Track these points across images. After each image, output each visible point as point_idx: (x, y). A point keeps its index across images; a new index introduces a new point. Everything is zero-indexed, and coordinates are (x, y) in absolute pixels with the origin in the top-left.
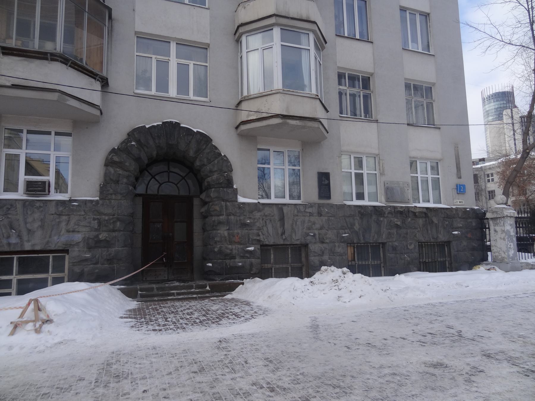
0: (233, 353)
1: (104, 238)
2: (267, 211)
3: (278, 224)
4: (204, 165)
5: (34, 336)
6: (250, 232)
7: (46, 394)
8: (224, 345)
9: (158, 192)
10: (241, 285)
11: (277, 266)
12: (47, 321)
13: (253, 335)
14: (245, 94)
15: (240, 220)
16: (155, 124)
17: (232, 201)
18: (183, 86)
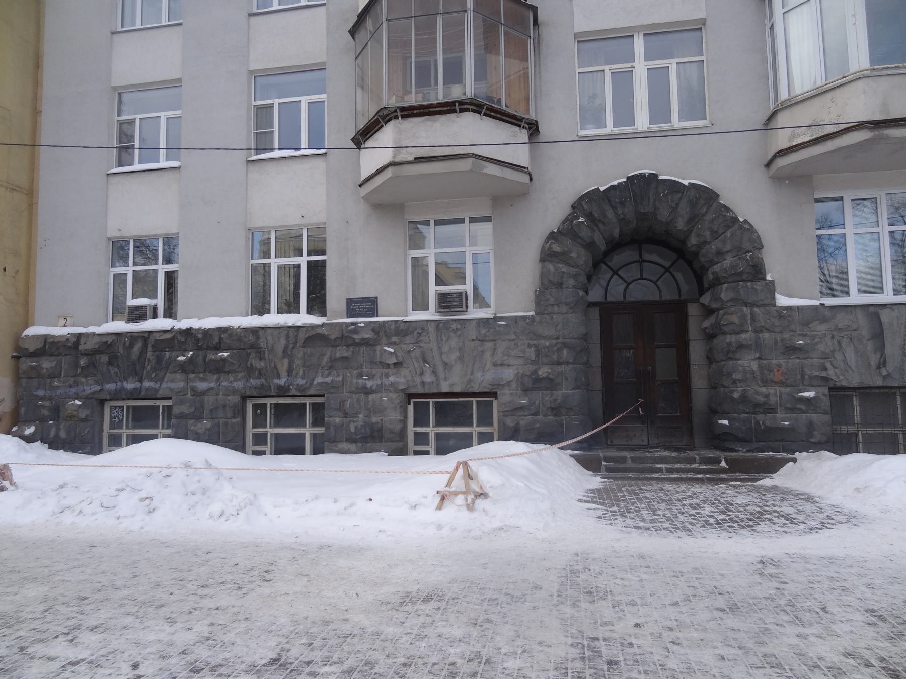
0: (791, 587)
1: (545, 375)
2: (842, 320)
3: (870, 346)
4: (705, 243)
5: (465, 513)
6: (806, 361)
7: (493, 600)
8: (771, 570)
9: (625, 298)
10: (791, 464)
11: (870, 430)
12: (481, 494)
13: (832, 561)
14: (784, 95)
15: (782, 340)
16: (615, 183)
17: (764, 305)
18: (659, 110)
